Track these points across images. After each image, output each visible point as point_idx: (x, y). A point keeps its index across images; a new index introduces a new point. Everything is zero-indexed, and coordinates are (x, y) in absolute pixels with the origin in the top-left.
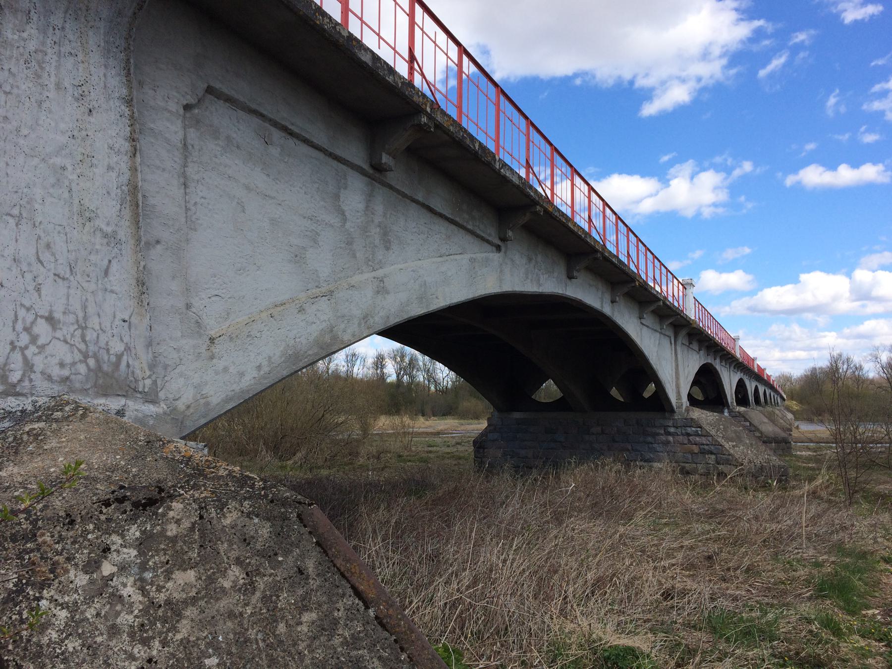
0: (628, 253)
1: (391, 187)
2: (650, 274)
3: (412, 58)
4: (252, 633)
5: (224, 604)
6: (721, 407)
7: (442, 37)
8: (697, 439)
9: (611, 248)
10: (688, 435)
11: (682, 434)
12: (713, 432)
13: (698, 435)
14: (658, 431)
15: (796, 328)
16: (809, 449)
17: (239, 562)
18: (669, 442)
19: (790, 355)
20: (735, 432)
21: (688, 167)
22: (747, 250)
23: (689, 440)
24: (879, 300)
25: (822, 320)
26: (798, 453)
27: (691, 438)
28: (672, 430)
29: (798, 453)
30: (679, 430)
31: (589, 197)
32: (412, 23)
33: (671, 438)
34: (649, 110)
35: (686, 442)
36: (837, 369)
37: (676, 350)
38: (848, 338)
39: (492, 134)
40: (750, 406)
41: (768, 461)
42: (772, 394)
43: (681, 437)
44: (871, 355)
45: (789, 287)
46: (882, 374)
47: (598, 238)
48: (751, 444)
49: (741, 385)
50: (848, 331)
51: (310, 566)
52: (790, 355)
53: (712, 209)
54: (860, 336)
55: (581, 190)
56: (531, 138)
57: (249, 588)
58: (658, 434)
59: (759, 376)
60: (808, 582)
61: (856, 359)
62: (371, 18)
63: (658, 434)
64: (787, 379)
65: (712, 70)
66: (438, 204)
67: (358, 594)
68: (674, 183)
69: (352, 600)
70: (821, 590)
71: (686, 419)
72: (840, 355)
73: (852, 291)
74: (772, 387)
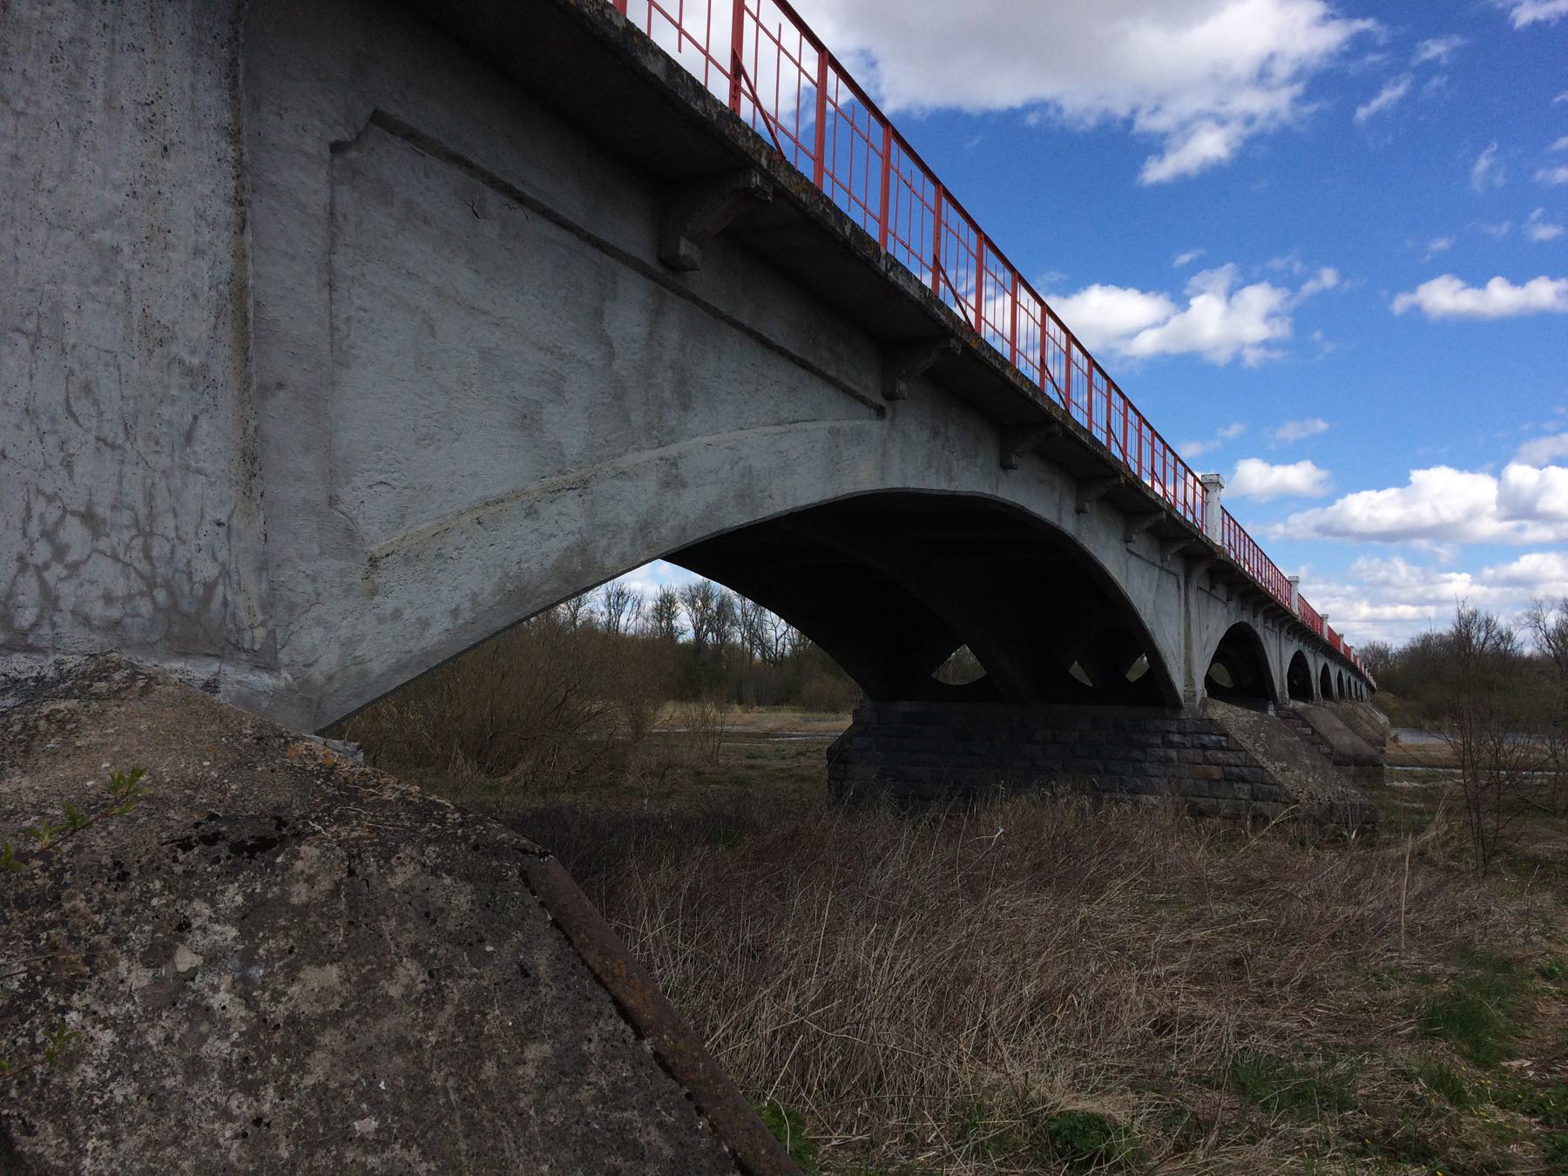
0: (1153, 469)
1: (694, 299)
2: (1146, 464)
3: (737, 71)
4: (437, 1078)
7: (791, 35)
8: (1220, 755)
9: (1079, 416)
10: (1204, 747)
11: (1194, 747)
12: (1248, 744)
13: (1221, 749)
17: (416, 952)
18: (1169, 760)
23: (1205, 756)
25: (1445, 552)
26: (1396, 783)
27: (1208, 753)
28: (1176, 738)
29: (1396, 783)
30: (1188, 738)
31: (1043, 326)
32: (887, 169)
33: (1173, 753)
35: (1199, 760)
37: (1187, 598)
38: (1490, 584)
39: (875, 208)
40: (1312, 700)
41: (1344, 796)
43: (1191, 752)
47: (1056, 398)
48: (1314, 767)
49: (1299, 662)
51: (542, 962)
55: (1029, 313)
58: (1152, 745)
59: (1331, 647)
61: (1503, 622)
63: (1152, 745)
66: (777, 331)
67: (624, 1013)
71: (1200, 720)
74: (1352, 668)
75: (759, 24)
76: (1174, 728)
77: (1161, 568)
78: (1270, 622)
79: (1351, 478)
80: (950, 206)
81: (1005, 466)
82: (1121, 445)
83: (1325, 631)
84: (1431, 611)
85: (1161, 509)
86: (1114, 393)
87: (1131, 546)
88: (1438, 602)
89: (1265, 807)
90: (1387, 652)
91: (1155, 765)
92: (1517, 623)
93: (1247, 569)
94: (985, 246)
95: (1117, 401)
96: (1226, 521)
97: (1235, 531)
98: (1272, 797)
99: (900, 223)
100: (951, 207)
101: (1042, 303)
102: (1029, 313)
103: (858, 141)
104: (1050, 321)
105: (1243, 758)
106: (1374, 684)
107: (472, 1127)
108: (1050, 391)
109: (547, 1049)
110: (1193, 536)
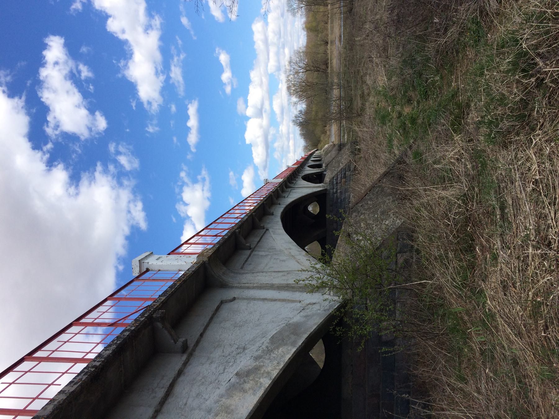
4: (372, 211)
5: (367, 217)
6: (323, 175)
7: (63, 337)
8: (339, 179)
10: (337, 183)
11: (337, 186)
12: (336, 172)
13: (337, 179)
14: (335, 197)
15: (276, 145)
16: (344, 136)
17: (360, 217)
18: (341, 192)
19: (292, 148)
20: (335, 163)
21: (180, 208)
22: (231, 174)
23: (339, 183)
24: (262, 104)
25: (272, 131)
26: (346, 140)
27: (338, 182)
28: (335, 190)
29: (346, 140)
30: (335, 187)
31: (191, 244)
33: (339, 191)
34: (143, 225)
35: (340, 184)
36: (301, 122)
37: (297, 188)
38: (283, 119)
40: (322, 164)
41: (348, 149)
42: (314, 155)
43: (338, 186)
44: (294, 106)
45: (253, 149)
46: (304, 101)
48: (341, 156)
49: (308, 178)
50: (279, 119)
51: (360, 205)
52: (292, 148)
53: (205, 192)
54: (282, 113)
55: (186, 249)
56: (220, 222)
57: (364, 214)
58: (337, 196)
59: (301, 165)
60: (382, 127)
62: (88, 348)
63: (337, 196)
64: (306, 148)
65: (125, 195)
66: (170, 374)
67: (366, 195)
68: (190, 214)
69: (366, 196)
70: (384, 123)
71: (330, 184)
72: (294, 121)
73: (256, 117)
75: (56, 350)
76: (332, 191)
77: (290, 192)
78: (293, 181)
79: (247, 158)
80: (87, 317)
81: (272, 214)
82: (222, 231)
83: (301, 160)
84: (291, 136)
85: (277, 189)
86: (217, 221)
87: (286, 197)
88: (289, 133)
89: (352, 168)
90: (305, 146)
91: (342, 196)
92: (296, 109)
93: (271, 190)
94: (140, 278)
95: (236, 208)
96: (259, 192)
97: (258, 193)
98: (349, 167)
99: (148, 295)
100: (88, 316)
101: (183, 244)
102: (186, 249)
103: (139, 288)
104: (190, 242)
105: (339, 173)
106: (316, 149)
107: (376, 206)
108: (224, 234)
109: (369, 202)
110: (263, 204)
